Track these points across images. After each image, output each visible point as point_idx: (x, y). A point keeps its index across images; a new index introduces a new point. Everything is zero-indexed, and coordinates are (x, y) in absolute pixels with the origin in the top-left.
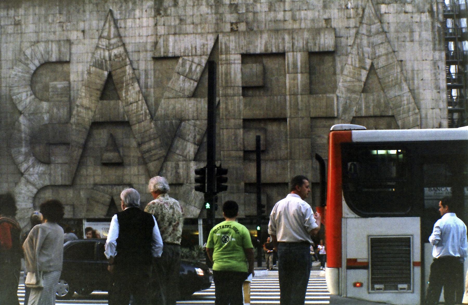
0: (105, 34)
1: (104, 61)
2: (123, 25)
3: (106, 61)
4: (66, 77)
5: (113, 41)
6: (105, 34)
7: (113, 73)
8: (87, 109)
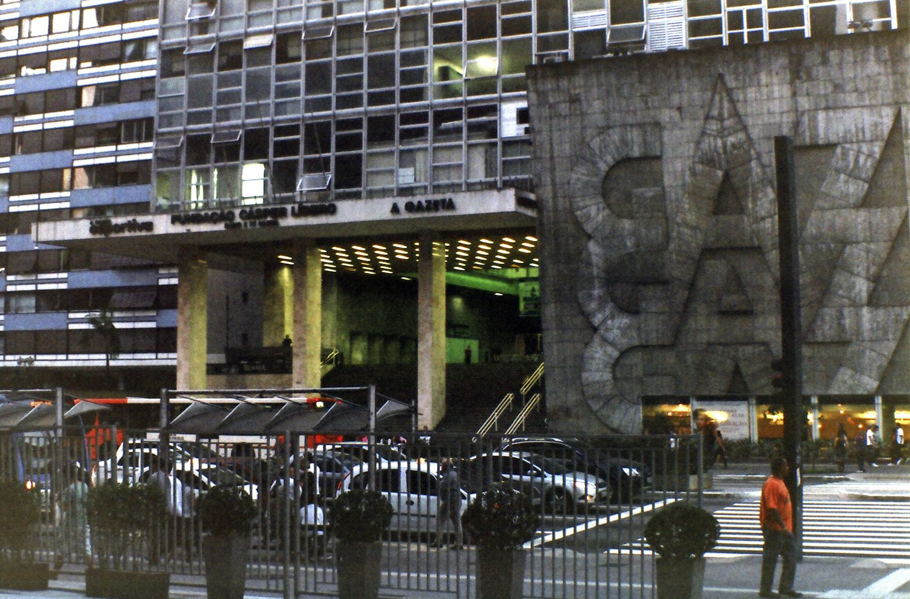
0: (715, 113)
1: (715, 154)
2: (741, 97)
3: (718, 154)
4: (658, 180)
5: (728, 123)
6: (715, 113)
7: (731, 173)
8: (694, 228)
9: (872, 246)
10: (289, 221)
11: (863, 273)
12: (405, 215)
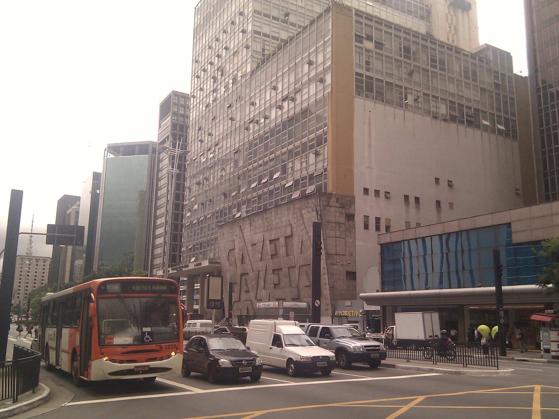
10: (184, 269)
12: (196, 267)
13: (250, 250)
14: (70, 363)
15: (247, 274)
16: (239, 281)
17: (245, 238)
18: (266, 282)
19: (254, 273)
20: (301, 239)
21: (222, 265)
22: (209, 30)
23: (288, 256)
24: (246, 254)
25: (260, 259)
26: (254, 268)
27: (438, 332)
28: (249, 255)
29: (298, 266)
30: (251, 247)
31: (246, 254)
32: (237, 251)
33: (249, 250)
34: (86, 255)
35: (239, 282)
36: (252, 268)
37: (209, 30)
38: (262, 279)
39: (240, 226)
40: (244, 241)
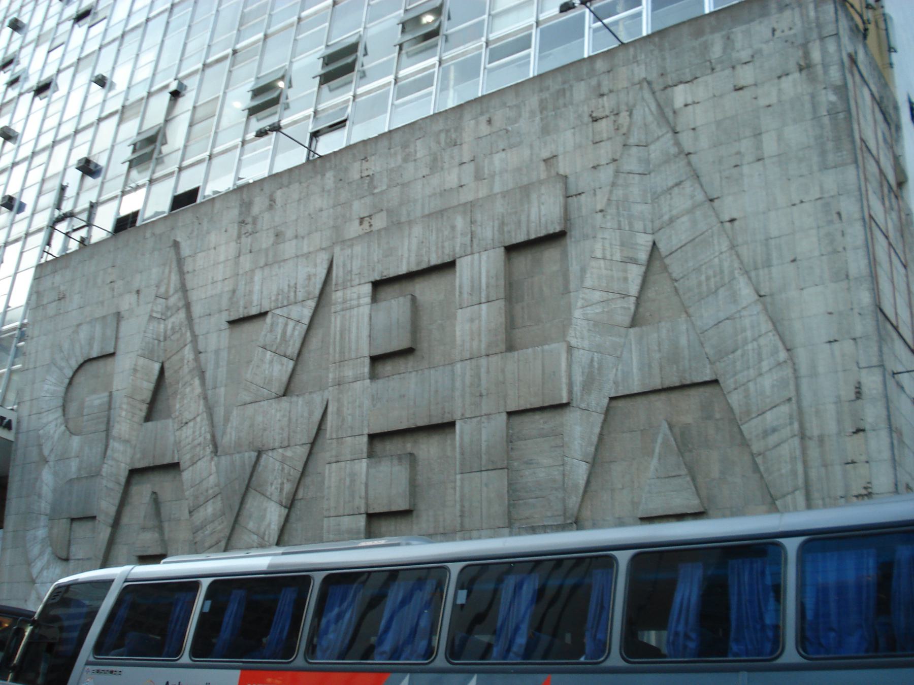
9: (289, 453)
11: (276, 497)
13: (217, 352)
14: (254, 320)
15: (174, 467)
16: (107, 506)
17: (194, 296)
18: (299, 505)
19: (224, 460)
20: (644, 241)
21: (22, 438)
22: (34, 9)
23: (511, 347)
24: (186, 369)
25: (277, 387)
26: (228, 438)
27: (639, 633)
28: (202, 374)
29: (598, 400)
30: (226, 334)
31: (186, 369)
32: (124, 363)
33: (212, 346)
34: (650, 628)
35: (112, 510)
36: (213, 437)
37: (34, 9)
38: (272, 490)
39: (176, 245)
40: (188, 306)
